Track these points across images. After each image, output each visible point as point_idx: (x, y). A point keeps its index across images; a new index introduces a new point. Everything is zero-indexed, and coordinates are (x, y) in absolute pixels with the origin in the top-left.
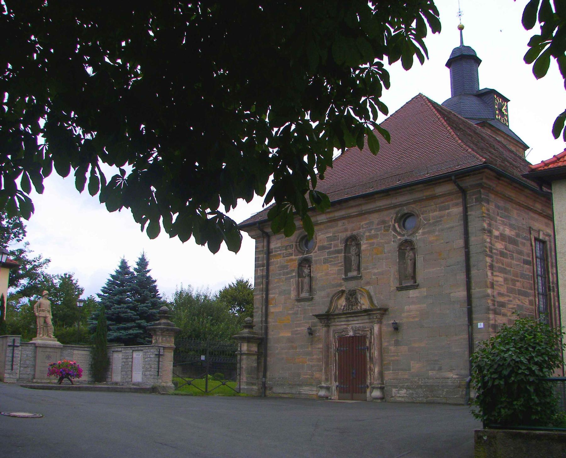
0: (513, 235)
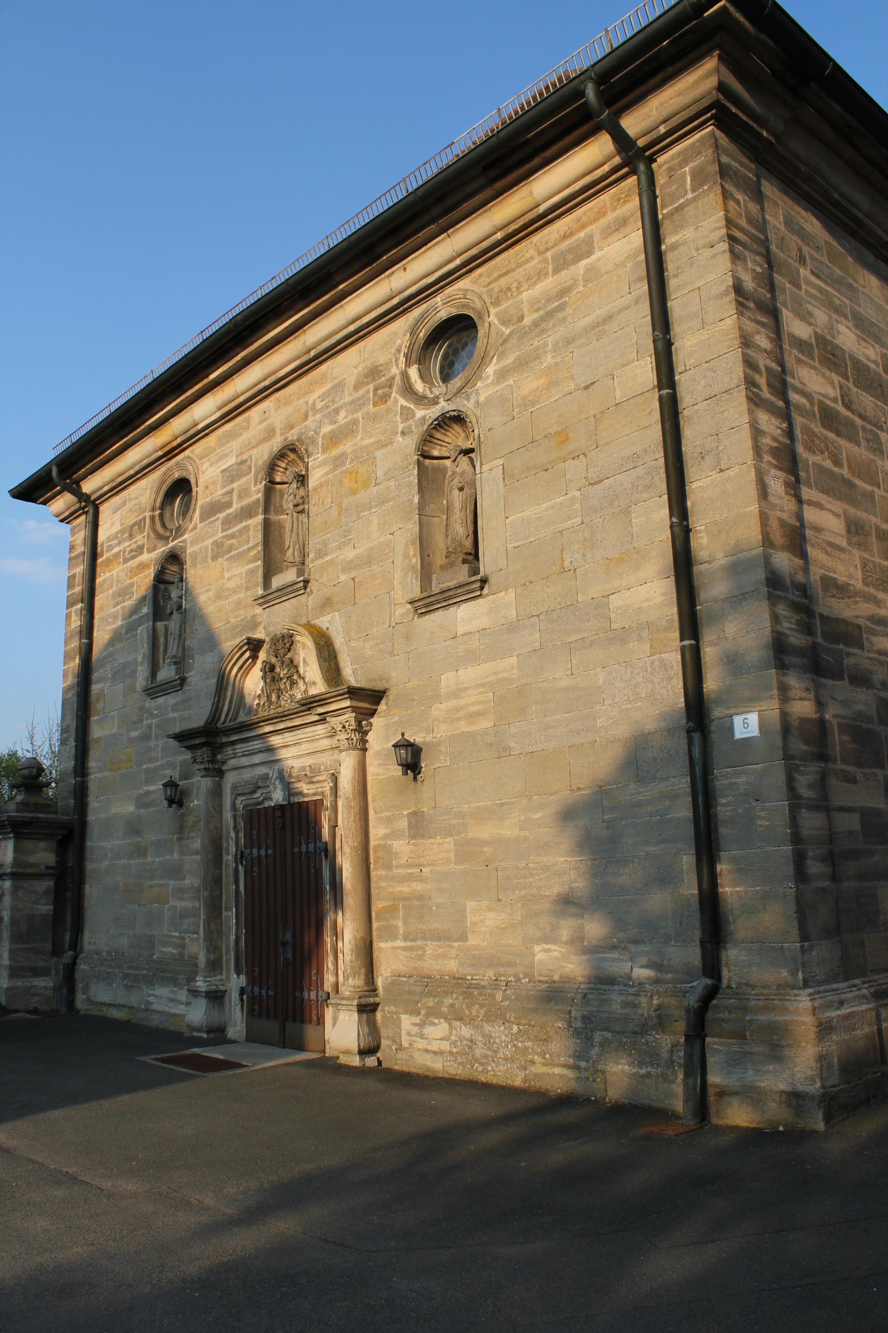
0: (875, 362)
